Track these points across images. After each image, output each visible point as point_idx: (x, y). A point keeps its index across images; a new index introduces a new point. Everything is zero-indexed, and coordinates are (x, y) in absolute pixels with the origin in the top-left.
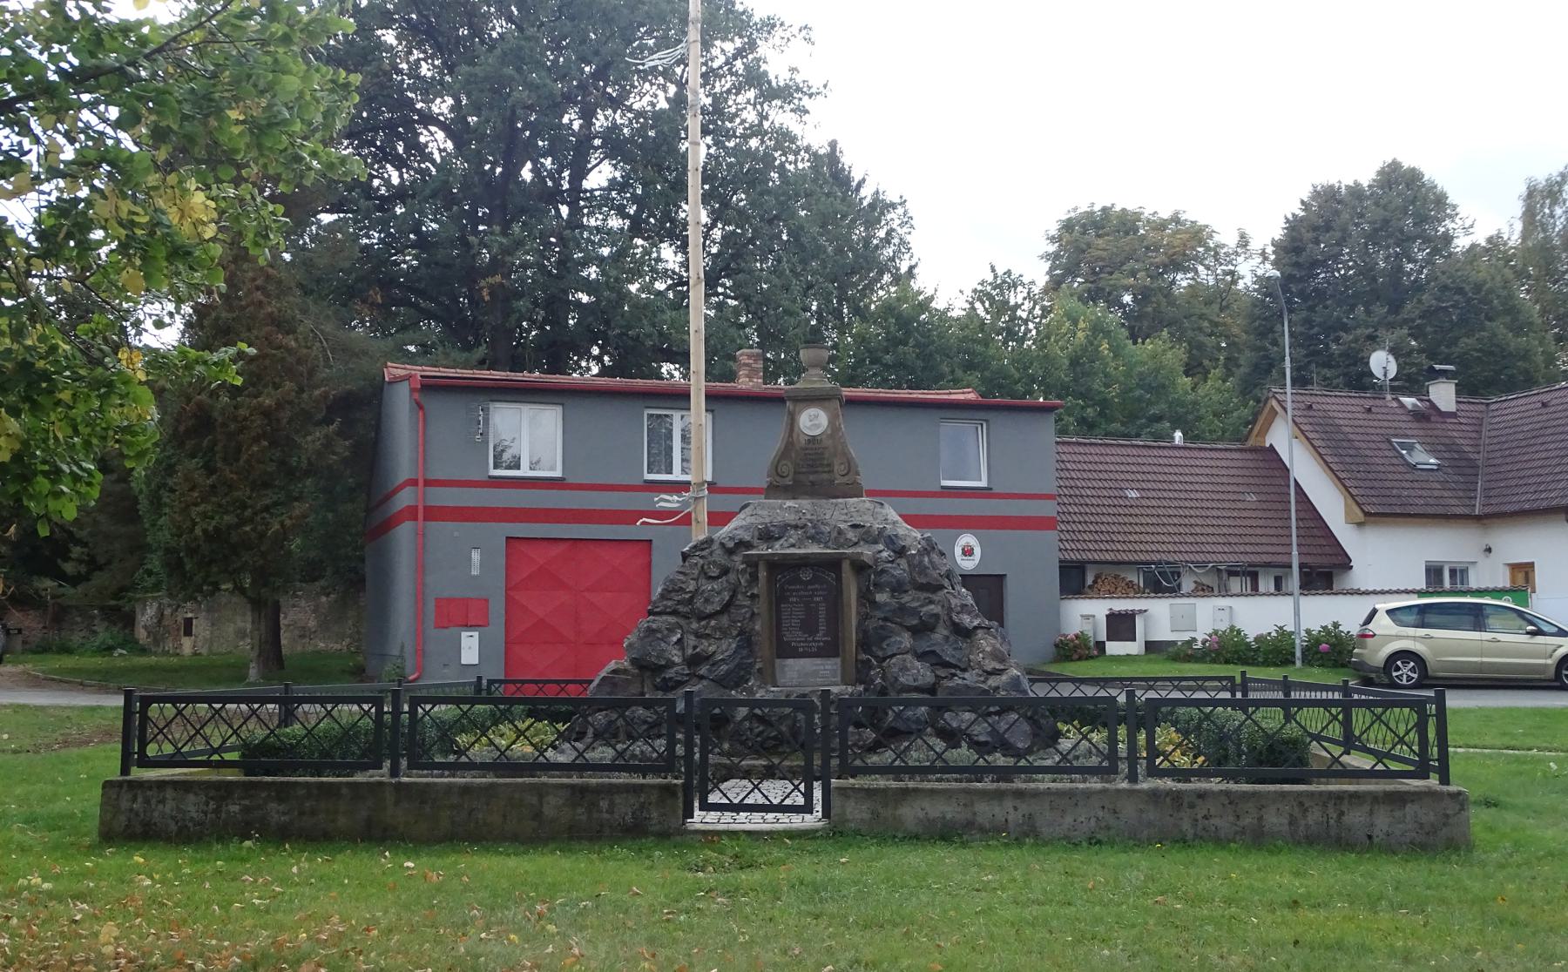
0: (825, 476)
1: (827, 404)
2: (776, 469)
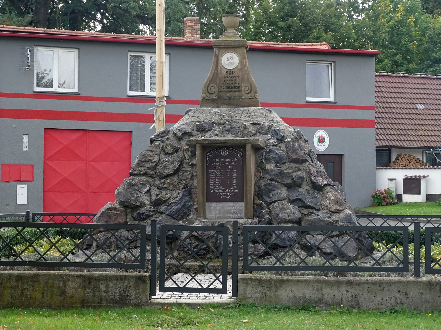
1: (238, 50)
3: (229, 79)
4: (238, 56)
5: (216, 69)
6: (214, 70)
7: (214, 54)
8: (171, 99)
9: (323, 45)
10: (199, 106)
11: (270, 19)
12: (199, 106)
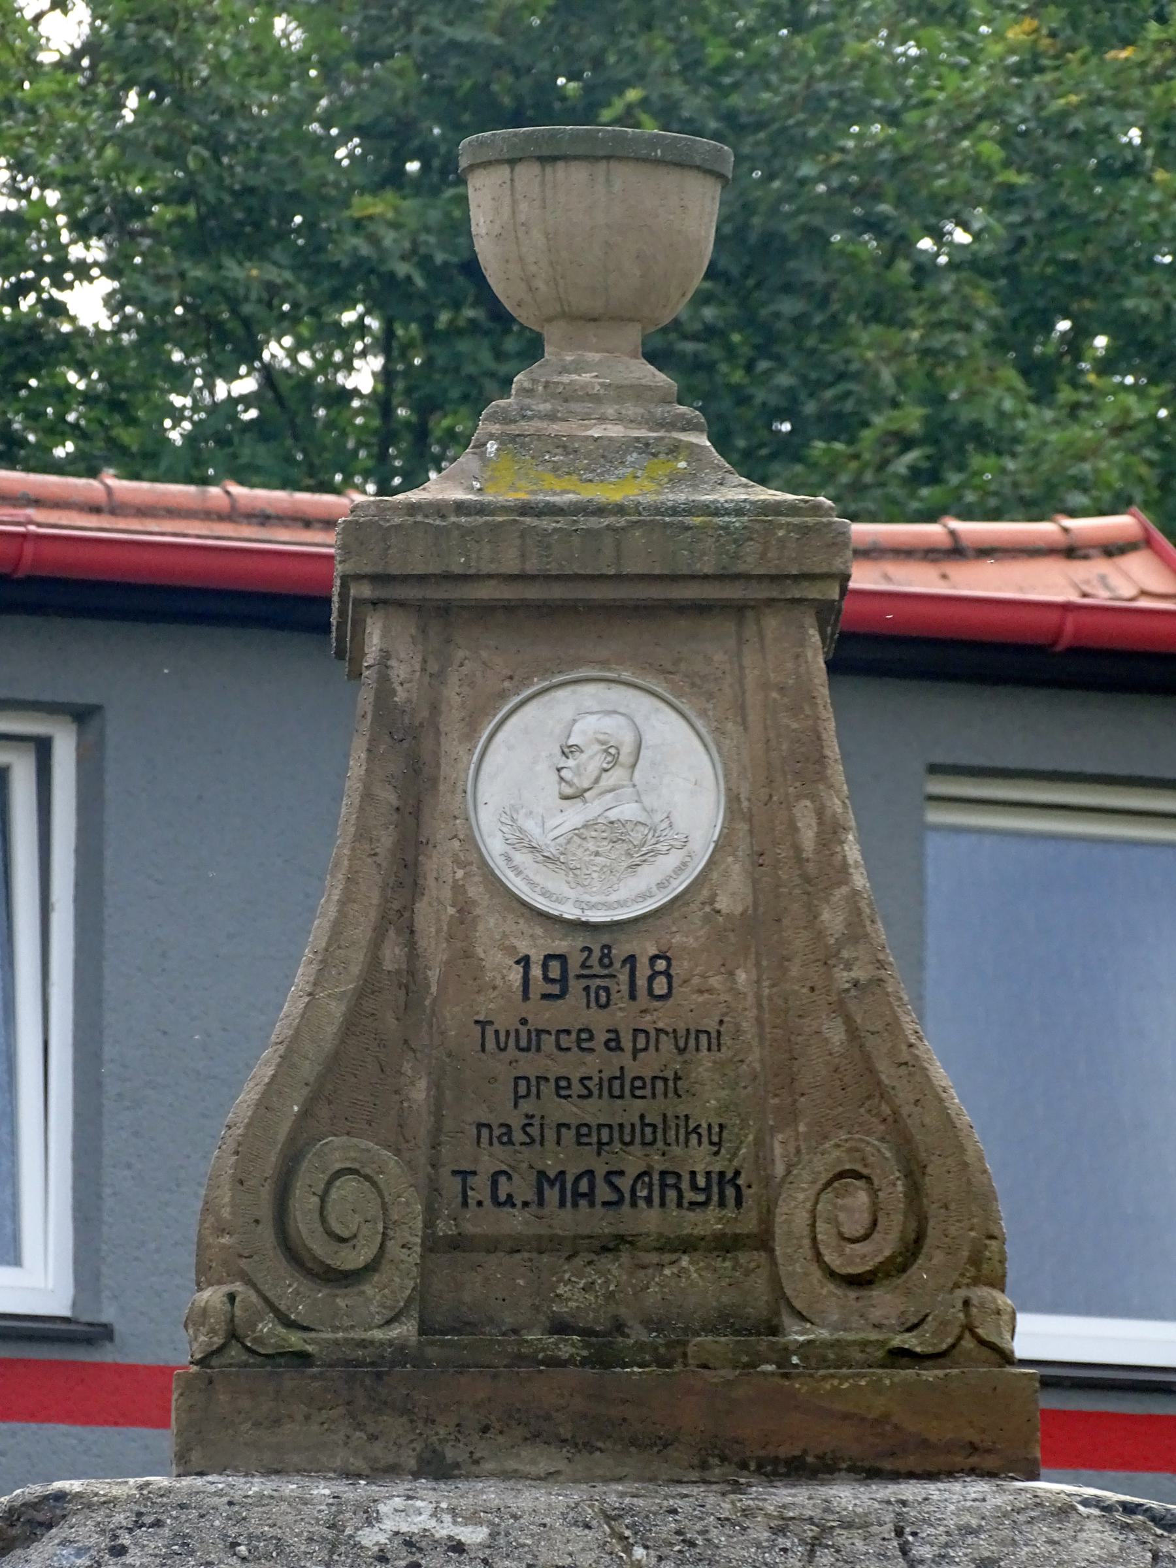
0: (695, 1283)
1: (713, 649)
2: (276, 1214)
3: (575, 1066)
4: (716, 738)
5: (398, 914)
6: (361, 933)
7: (366, 698)
8: (107, 1355)
9: (1113, 550)
10: (164, 1441)
11: (217, 146)
12: (164, 1441)
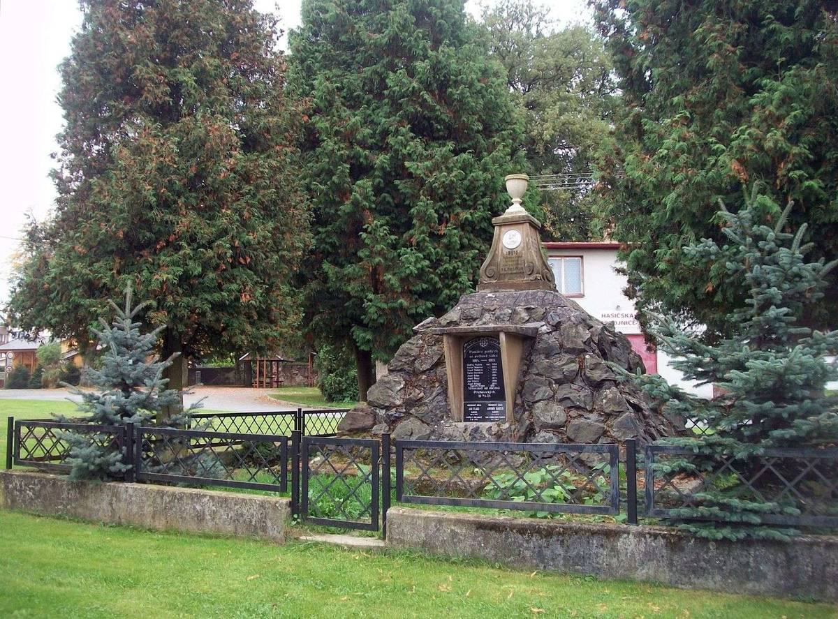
1: (520, 226)
